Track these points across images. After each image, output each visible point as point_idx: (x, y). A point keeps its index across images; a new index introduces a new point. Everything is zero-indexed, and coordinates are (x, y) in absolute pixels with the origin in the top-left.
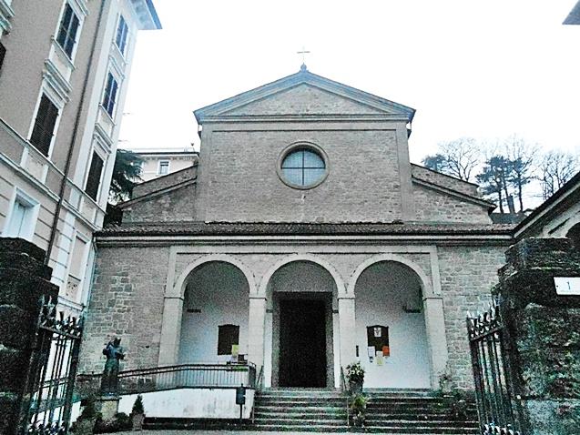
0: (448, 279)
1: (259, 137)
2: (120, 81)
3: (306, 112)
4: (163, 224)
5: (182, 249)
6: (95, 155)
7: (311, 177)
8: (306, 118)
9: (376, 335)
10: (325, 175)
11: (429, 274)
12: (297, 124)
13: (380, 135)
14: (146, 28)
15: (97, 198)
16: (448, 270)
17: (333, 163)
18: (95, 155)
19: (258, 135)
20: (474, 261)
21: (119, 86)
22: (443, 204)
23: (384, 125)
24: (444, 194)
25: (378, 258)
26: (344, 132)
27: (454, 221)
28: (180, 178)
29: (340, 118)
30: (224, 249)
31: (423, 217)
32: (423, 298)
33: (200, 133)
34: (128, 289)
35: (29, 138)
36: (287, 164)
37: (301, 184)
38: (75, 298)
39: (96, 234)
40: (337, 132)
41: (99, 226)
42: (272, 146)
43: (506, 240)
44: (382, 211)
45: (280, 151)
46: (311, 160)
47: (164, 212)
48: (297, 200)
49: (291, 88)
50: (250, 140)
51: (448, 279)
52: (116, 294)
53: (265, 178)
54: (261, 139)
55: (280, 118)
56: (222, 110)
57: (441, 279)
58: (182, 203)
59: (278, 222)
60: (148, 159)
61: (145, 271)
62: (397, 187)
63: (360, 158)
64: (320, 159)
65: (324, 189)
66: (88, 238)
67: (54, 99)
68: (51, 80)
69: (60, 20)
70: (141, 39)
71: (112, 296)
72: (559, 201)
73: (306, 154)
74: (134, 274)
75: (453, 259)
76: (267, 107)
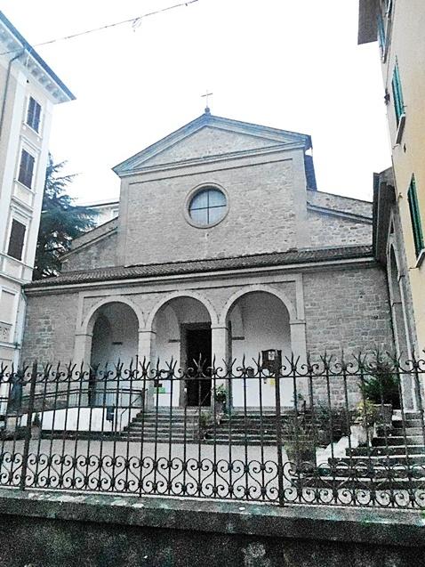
3: (208, 154)
4: (91, 271)
5: (88, 294)
7: (215, 215)
8: (205, 161)
9: (270, 358)
10: (225, 213)
11: (294, 302)
12: (200, 167)
13: (277, 166)
14: (62, 101)
20: (338, 285)
24: (338, 217)
25: (247, 290)
27: (349, 243)
28: (108, 230)
29: (238, 155)
30: (118, 291)
31: (317, 243)
34: (50, 330)
35: (6, 251)
38: (8, 339)
39: (23, 287)
42: (179, 191)
43: (368, 262)
44: (278, 241)
45: (186, 196)
46: (215, 199)
47: (93, 261)
48: (201, 239)
54: (169, 185)
55: (185, 164)
58: (106, 251)
60: (103, 209)
62: (293, 215)
65: (225, 226)
66: (18, 292)
67: (30, 152)
70: (53, 112)
73: (210, 192)
75: (318, 285)
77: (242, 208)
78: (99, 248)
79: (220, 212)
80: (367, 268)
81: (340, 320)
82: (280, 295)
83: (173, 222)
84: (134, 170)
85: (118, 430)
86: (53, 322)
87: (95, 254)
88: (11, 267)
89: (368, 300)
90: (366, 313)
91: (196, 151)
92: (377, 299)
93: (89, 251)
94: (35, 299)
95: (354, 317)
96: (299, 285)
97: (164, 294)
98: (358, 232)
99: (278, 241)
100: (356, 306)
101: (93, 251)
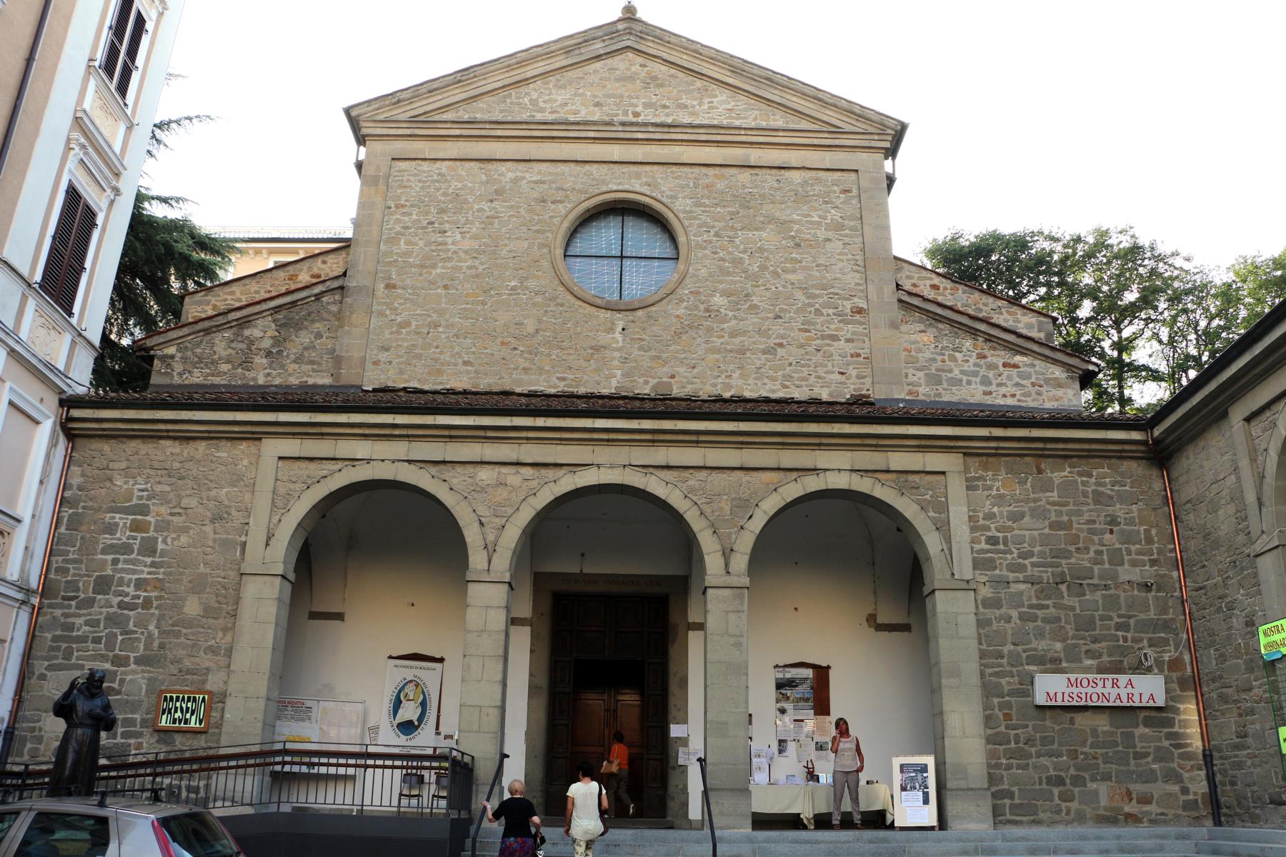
0: (992, 541)
1: (510, 175)
2: (154, 14)
3: (631, 118)
5: (291, 447)
6: (73, 195)
7: (639, 281)
8: (626, 133)
11: (943, 527)
15: (76, 309)
16: (990, 516)
17: (699, 247)
18: (73, 195)
19: (508, 173)
21: (149, 26)
22: (973, 360)
23: (828, 159)
24: (974, 332)
25: (813, 484)
26: (648, 168)
27: (1000, 401)
28: (304, 278)
32: (926, 590)
33: (359, 166)
34: (149, 548)
35: (38, 277)
36: (579, 246)
37: (616, 296)
39: (68, 402)
40: (711, 171)
41: (81, 377)
45: (565, 215)
46: (641, 238)
47: (260, 360)
48: (604, 338)
49: (598, 58)
50: (487, 182)
51: (992, 541)
52: (115, 562)
53: (523, 279)
54: (515, 181)
56: (420, 107)
57: (973, 542)
58: (305, 338)
61: (193, 502)
62: (860, 311)
63: (767, 236)
67: (90, 193)
68: (86, 154)
71: (103, 567)
72: (1240, 384)
73: (631, 222)
74: (164, 510)
76: (532, 101)
77: (724, 272)
78: (281, 326)
79: (662, 274)
80: (1121, 456)
81: (1063, 587)
82: (906, 507)
83: (523, 279)
84: (414, 120)
86: (163, 526)
87: (267, 344)
88: (43, 332)
89: (1128, 538)
90: (1127, 573)
91: (597, 104)
92: (1149, 540)
93: (247, 332)
94: (95, 445)
95: (1095, 581)
96: (956, 488)
97: (550, 473)
98: (1020, 376)
99: (821, 372)
100: (1099, 553)
101: (262, 331)
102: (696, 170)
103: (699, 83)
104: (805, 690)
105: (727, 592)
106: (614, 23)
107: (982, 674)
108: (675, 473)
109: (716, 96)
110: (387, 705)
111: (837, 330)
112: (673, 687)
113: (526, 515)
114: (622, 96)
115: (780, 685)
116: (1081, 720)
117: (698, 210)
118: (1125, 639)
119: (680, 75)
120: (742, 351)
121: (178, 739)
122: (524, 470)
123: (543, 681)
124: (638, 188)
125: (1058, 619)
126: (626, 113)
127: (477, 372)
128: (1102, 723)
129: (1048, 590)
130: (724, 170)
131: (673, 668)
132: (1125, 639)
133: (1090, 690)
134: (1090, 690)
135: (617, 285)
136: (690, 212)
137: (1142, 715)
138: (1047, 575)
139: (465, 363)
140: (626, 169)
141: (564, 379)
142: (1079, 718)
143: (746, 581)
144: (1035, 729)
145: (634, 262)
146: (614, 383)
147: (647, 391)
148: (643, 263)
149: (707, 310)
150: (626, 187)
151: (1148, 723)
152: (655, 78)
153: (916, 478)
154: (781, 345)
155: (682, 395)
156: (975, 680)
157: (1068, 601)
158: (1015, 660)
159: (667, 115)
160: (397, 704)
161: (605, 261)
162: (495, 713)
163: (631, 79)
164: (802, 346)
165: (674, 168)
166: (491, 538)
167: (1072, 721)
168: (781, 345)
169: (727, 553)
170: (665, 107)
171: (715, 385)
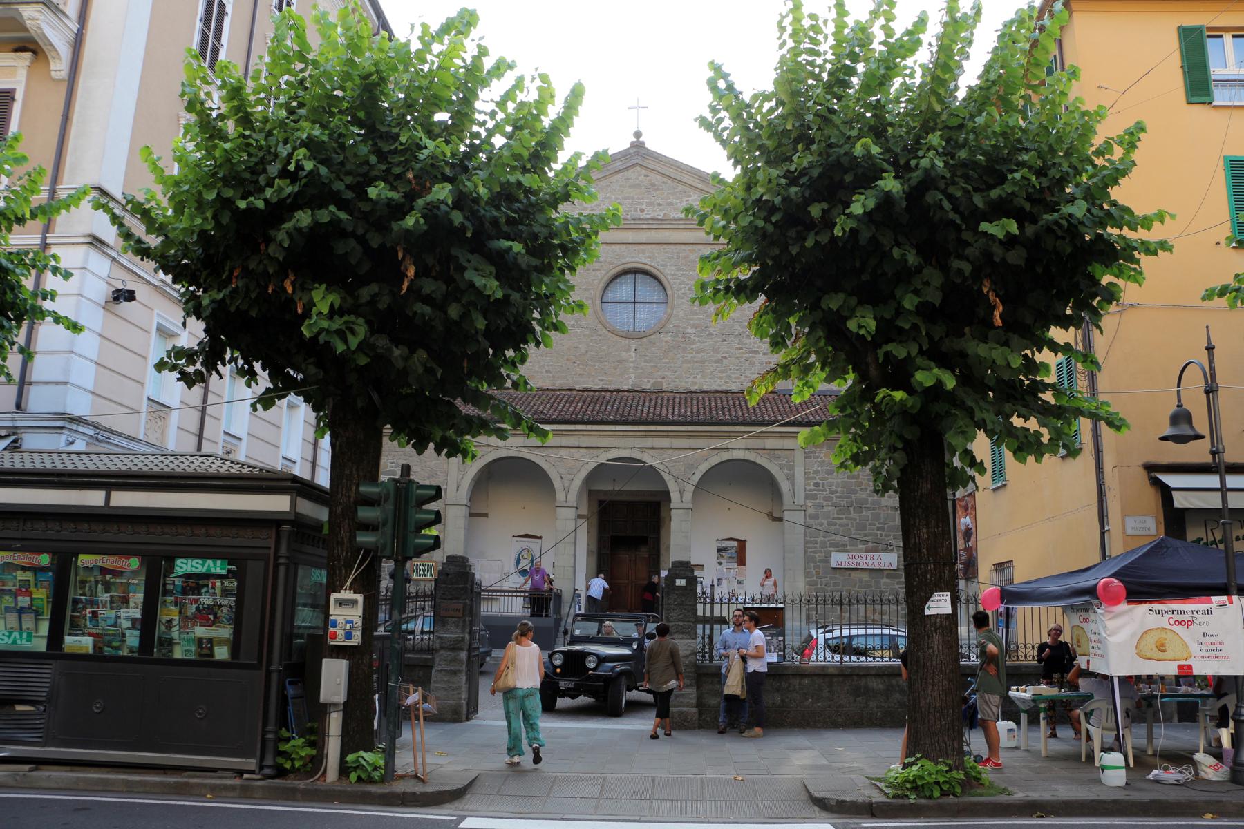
7: (647, 317)
11: (791, 479)
16: (816, 472)
25: (726, 456)
26: (649, 246)
36: (610, 296)
46: (646, 290)
48: (624, 355)
49: (618, 172)
51: (817, 485)
57: (806, 485)
59: (596, 388)
64: (657, 283)
69: (199, 17)
73: (639, 276)
81: (851, 509)
82: (773, 468)
85: (326, 555)
97: (595, 452)
102: (678, 246)
103: (680, 188)
104: (733, 553)
105: (681, 511)
106: (628, 149)
107: (806, 552)
108: (657, 451)
109: (690, 196)
110: (513, 562)
111: (758, 347)
112: (663, 551)
113: (583, 473)
114: (633, 198)
115: (719, 550)
116: (854, 575)
117: (679, 273)
118: (881, 535)
119: (669, 182)
120: (703, 362)
121: (422, 584)
122: (581, 450)
123: (594, 547)
124: (643, 260)
125: (847, 525)
126: (636, 210)
127: (553, 377)
128: (865, 577)
129: (842, 510)
130: (694, 246)
131: (663, 540)
132: (881, 535)
133: (859, 561)
134: (859, 561)
135: (632, 320)
136: (675, 275)
137: (886, 572)
138: (843, 502)
139: (547, 372)
140: (636, 247)
141: (602, 380)
142: (853, 574)
143: (690, 506)
144: (831, 578)
145: (642, 305)
146: (631, 382)
147: (648, 387)
148: (647, 305)
149: (683, 337)
150: (637, 260)
151: (888, 576)
152: (653, 185)
153: (779, 452)
154: (725, 358)
155: (669, 389)
156: (802, 555)
157: (853, 515)
158: (824, 545)
159: (661, 210)
160: (519, 561)
161: (625, 305)
162: (571, 570)
163: (638, 186)
164: (737, 358)
165: (665, 246)
166: (566, 485)
167: (850, 575)
168: (725, 358)
169: (682, 492)
170: (659, 205)
171: (687, 382)
